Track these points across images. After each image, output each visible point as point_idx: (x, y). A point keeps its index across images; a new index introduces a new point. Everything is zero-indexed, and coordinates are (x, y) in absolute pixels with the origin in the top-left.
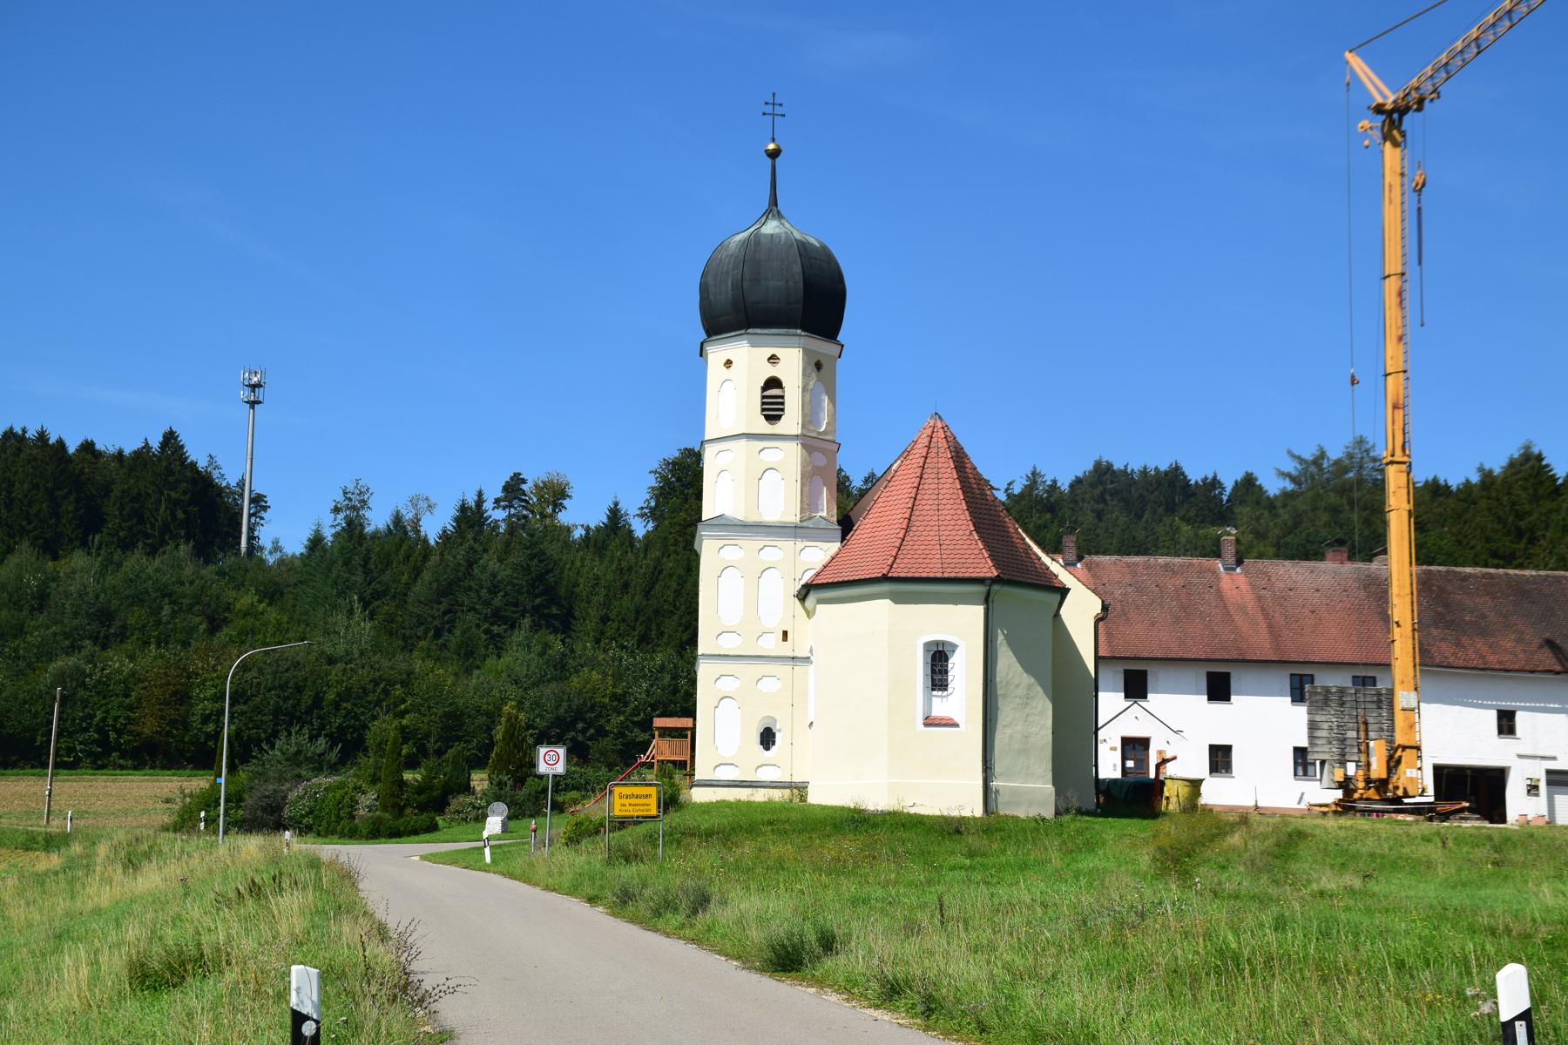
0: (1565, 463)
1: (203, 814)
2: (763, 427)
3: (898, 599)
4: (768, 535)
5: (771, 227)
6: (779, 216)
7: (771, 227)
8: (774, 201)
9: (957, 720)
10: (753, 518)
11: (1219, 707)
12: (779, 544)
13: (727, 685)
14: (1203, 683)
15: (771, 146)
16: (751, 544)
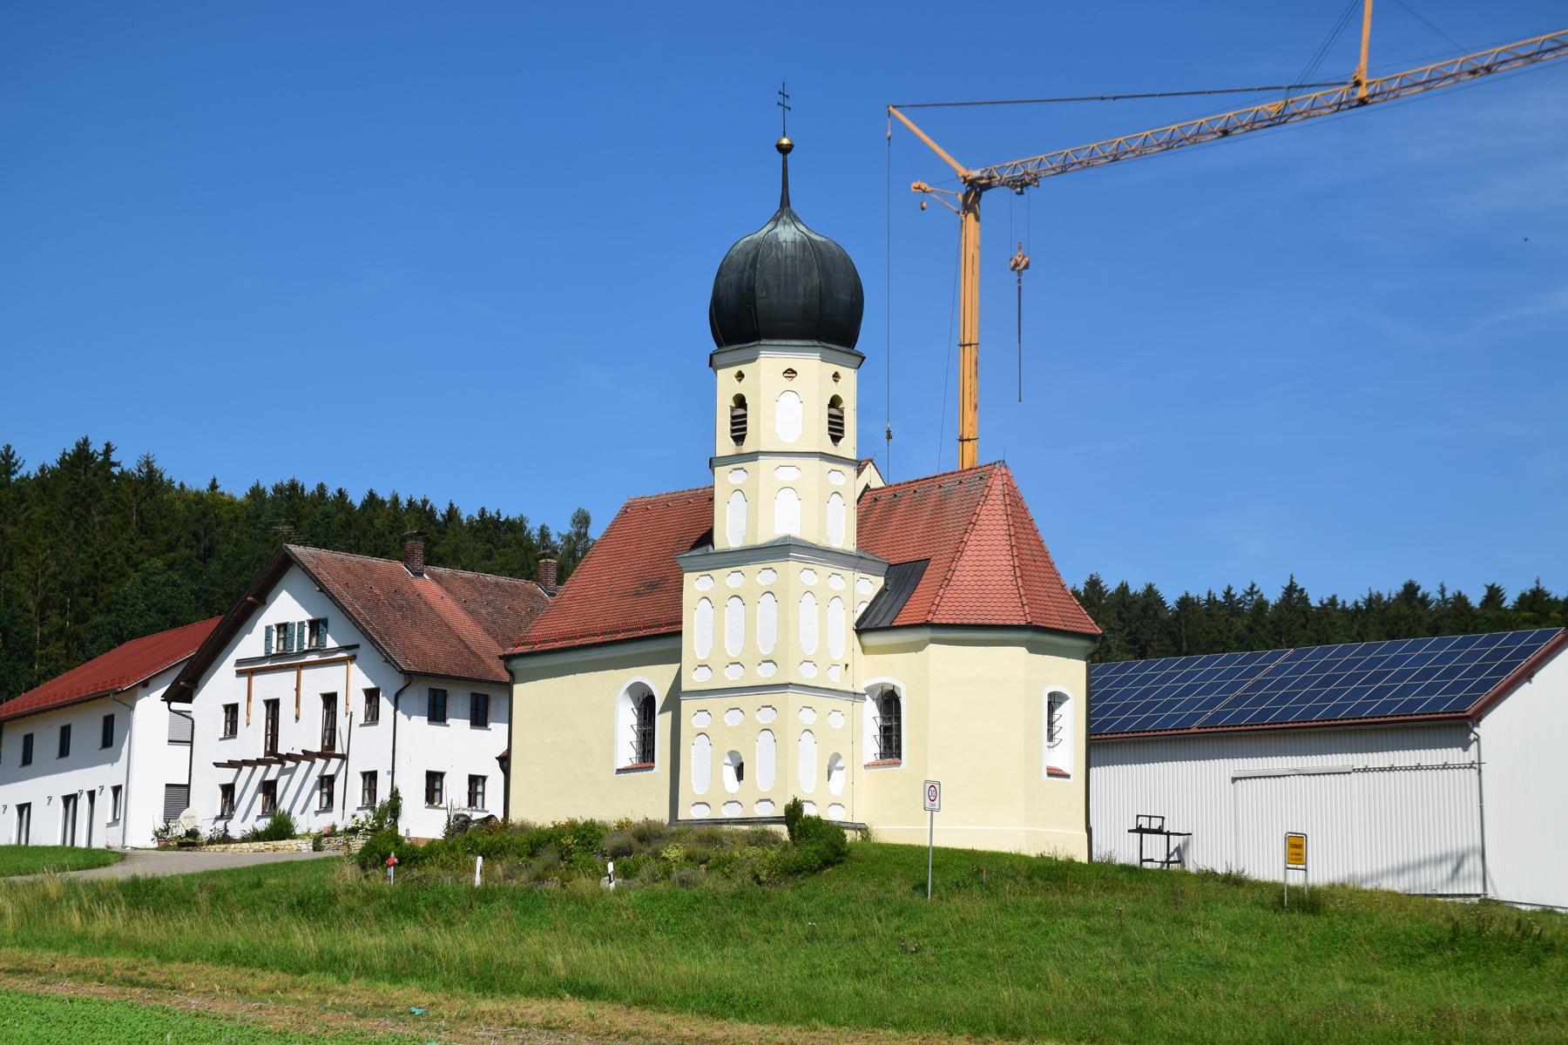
0: (1559, 590)
1: (611, 866)
2: (828, 446)
3: (1034, 648)
4: (836, 562)
5: (787, 233)
6: (795, 219)
7: (787, 233)
8: (785, 201)
9: (1067, 771)
10: (823, 543)
11: (437, 729)
12: (843, 572)
13: (808, 718)
14: (424, 704)
15: (785, 141)
16: (824, 570)
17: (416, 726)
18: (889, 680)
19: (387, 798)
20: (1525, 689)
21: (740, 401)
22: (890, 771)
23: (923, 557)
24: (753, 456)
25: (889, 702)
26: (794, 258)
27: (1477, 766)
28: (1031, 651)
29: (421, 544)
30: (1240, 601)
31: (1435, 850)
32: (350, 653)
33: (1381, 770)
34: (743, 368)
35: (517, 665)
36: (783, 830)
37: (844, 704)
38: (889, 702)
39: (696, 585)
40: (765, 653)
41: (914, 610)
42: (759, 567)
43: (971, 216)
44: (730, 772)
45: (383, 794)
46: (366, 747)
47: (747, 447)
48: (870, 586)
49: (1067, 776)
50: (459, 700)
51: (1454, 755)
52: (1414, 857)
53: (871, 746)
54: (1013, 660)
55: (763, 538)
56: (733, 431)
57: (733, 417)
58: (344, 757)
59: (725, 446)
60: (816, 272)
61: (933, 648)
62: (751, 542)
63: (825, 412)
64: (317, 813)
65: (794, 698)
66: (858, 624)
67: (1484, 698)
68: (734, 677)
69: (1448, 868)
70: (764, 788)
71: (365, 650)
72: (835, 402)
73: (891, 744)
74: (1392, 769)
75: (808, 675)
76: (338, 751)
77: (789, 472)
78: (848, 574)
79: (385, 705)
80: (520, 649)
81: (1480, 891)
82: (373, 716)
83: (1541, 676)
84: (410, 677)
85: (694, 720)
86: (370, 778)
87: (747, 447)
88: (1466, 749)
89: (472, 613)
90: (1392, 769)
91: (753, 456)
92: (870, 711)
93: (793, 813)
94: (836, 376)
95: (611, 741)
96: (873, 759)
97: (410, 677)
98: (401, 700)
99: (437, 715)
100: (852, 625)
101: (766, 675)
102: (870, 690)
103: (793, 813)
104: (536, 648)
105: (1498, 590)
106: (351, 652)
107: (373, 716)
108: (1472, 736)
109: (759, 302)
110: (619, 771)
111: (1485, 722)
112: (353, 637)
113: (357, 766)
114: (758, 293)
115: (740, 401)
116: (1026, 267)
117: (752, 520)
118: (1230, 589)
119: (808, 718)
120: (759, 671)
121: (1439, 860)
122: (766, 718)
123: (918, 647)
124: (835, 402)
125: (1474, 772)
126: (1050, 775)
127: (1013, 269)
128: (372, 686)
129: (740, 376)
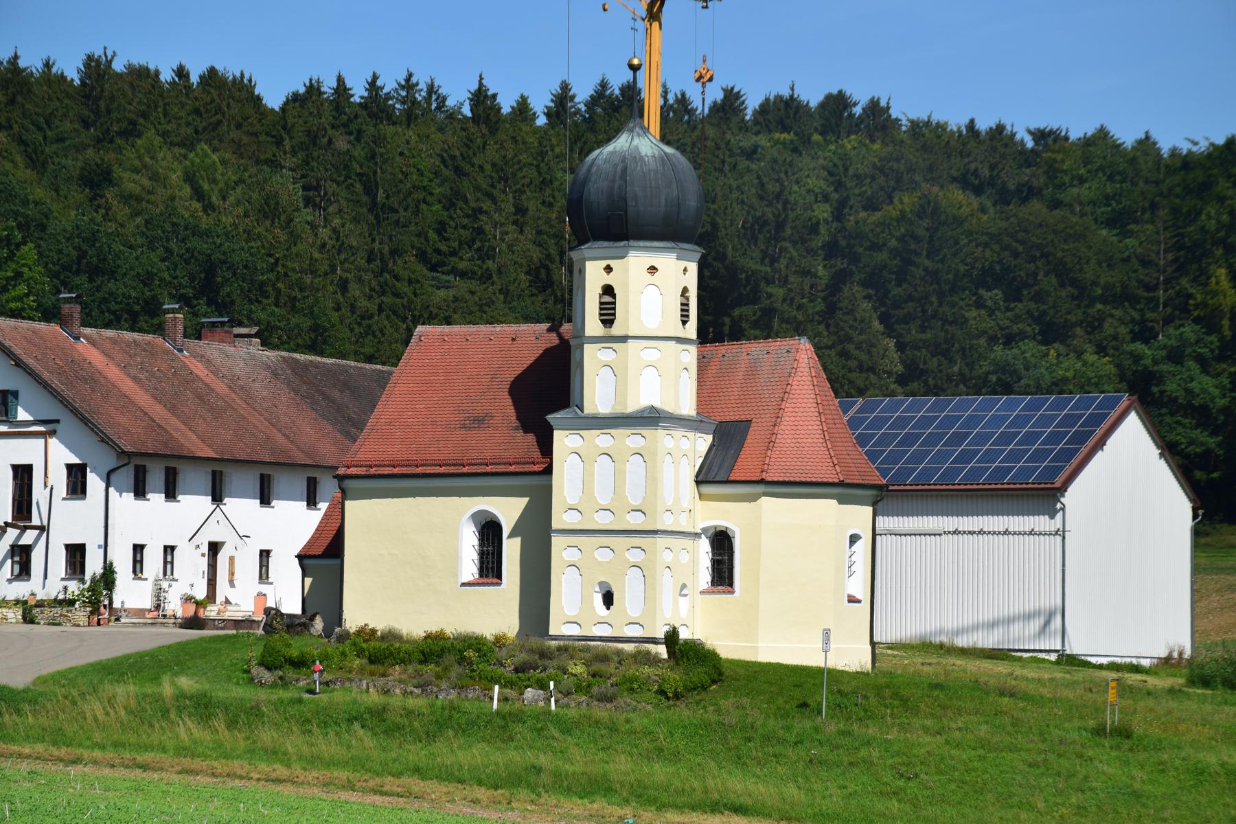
3: (842, 500)
4: (684, 427)
9: (859, 597)
11: (140, 503)
13: (668, 557)
15: (636, 62)
16: (678, 433)
17: (123, 501)
18: (721, 523)
19: (99, 570)
20: (1099, 457)
21: (608, 290)
22: (721, 599)
23: (743, 418)
24: (624, 339)
25: (722, 542)
26: (656, 172)
27: (1062, 533)
28: (840, 503)
29: (78, 308)
30: (388, 96)
31: (1030, 606)
32: (49, 427)
33: (970, 533)
34: (612, 263)
35: (349, 484)
36: (662, 651)
37: (687, 542)
38: (722, 542)
39: (566, 441)
40: (635, 503)
41: (746, 466)
42: (629, 431)
43: (656, 25)
44: (598, 599)
45: (94, 566)
46: (71, 521)
47: (616, 330)
48: (703, 442)
49: (859, 601)
50: (156, 476)
51: (1041, 522)
52: (1006, 612)
53: (704, 576)
54: (825, 509)
55: (631, 407)
56: (601, 315)
57: (601, 303)
58: (42, 529)
59: (593, 326)
60: (674, 185)
61: (765, 500)
62: (620, 410)
63: (679, 300)
64: (10, 581)
65: (661, 541)
66: (697, 476)
67: (1069, 469)
68: (603, 521)
69: (1036, 625)
70: (634, 612)
71: (68, 423)
72: (685, 290)
73: (723, 574)
74: (981, 532)
75: (667, 523)
76: (36, 521)
77: (650, 353)
78: (691, 434)
79: (94, 482)
80: (353, 471)
81: (1059, 647)
82: (77, 487)
83: (1110, 442)
84: (125, 456)
85: (564, 554)
86: (76, 553)
87: (616, 330)
88: (1052, 517)
89: (135, 379)
90: (981, 532)
91: (624, 339)
92: (704, 547)
93: (671, 638)
94: (685, 270)
95: (454, 558)
96: (706, 586)
97: (125, 456)
98: (113, 478)
99: (140, 492)
100: (693, 478)
101: (635, 521)
102: (705, 530)
103: (671, 638)
104: (373, 471)
105: (738, 96)
106: (51, 427)
107: (77, 487)
108: (1059, 506)
109: (630, 210)
110: (463, 585)
111: (1072, 489)
112: (51, 410)
113: (60, 537)
114: (629, 203)
115: (608, 290)
116: (711, 79)
117: (621, 391)
118: (375, 77)
119: (668, 557)
120: (628, 517)
121: (1029, 616)
122: (635, 556)
123: (753, 498)
124: (685, 290)
125: (1059, 539)
126: (850, 601)
127: (698, 80)
128: (76, 460)
129: (609, 269)
